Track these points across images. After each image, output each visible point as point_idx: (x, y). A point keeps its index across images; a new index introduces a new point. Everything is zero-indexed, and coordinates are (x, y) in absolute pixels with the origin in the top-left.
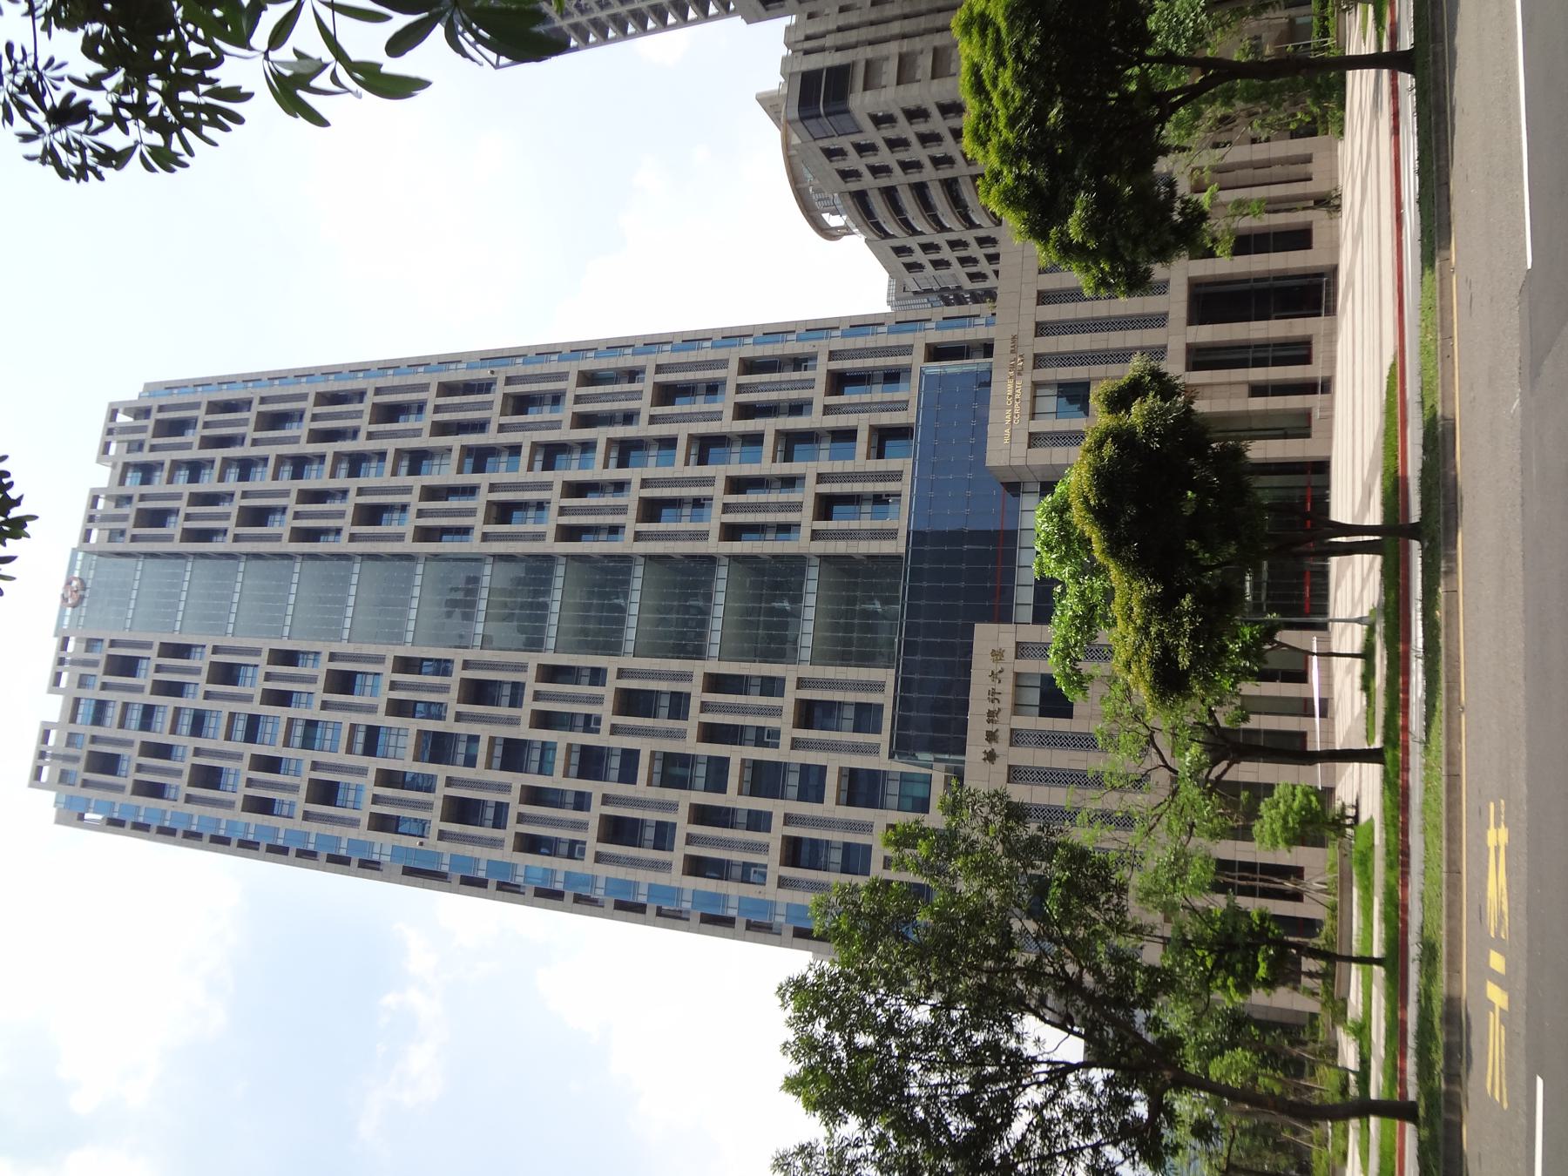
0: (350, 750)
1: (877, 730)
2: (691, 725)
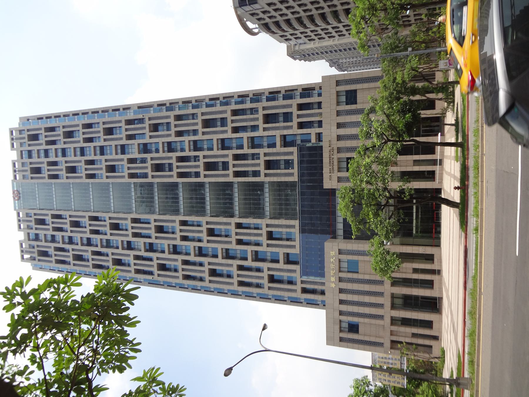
0: (116, 154)
1: (293, 168)
2: (231, 172)
